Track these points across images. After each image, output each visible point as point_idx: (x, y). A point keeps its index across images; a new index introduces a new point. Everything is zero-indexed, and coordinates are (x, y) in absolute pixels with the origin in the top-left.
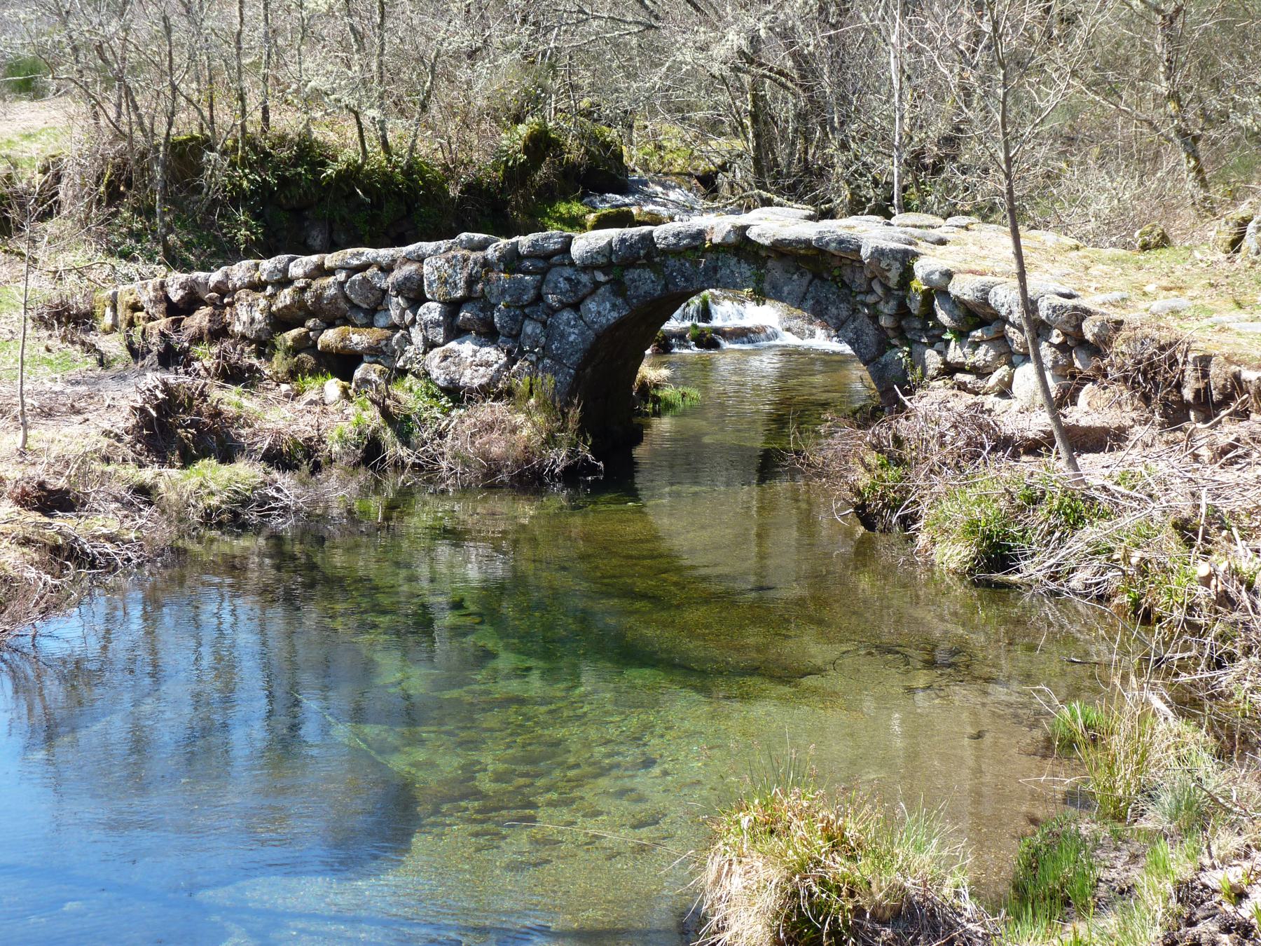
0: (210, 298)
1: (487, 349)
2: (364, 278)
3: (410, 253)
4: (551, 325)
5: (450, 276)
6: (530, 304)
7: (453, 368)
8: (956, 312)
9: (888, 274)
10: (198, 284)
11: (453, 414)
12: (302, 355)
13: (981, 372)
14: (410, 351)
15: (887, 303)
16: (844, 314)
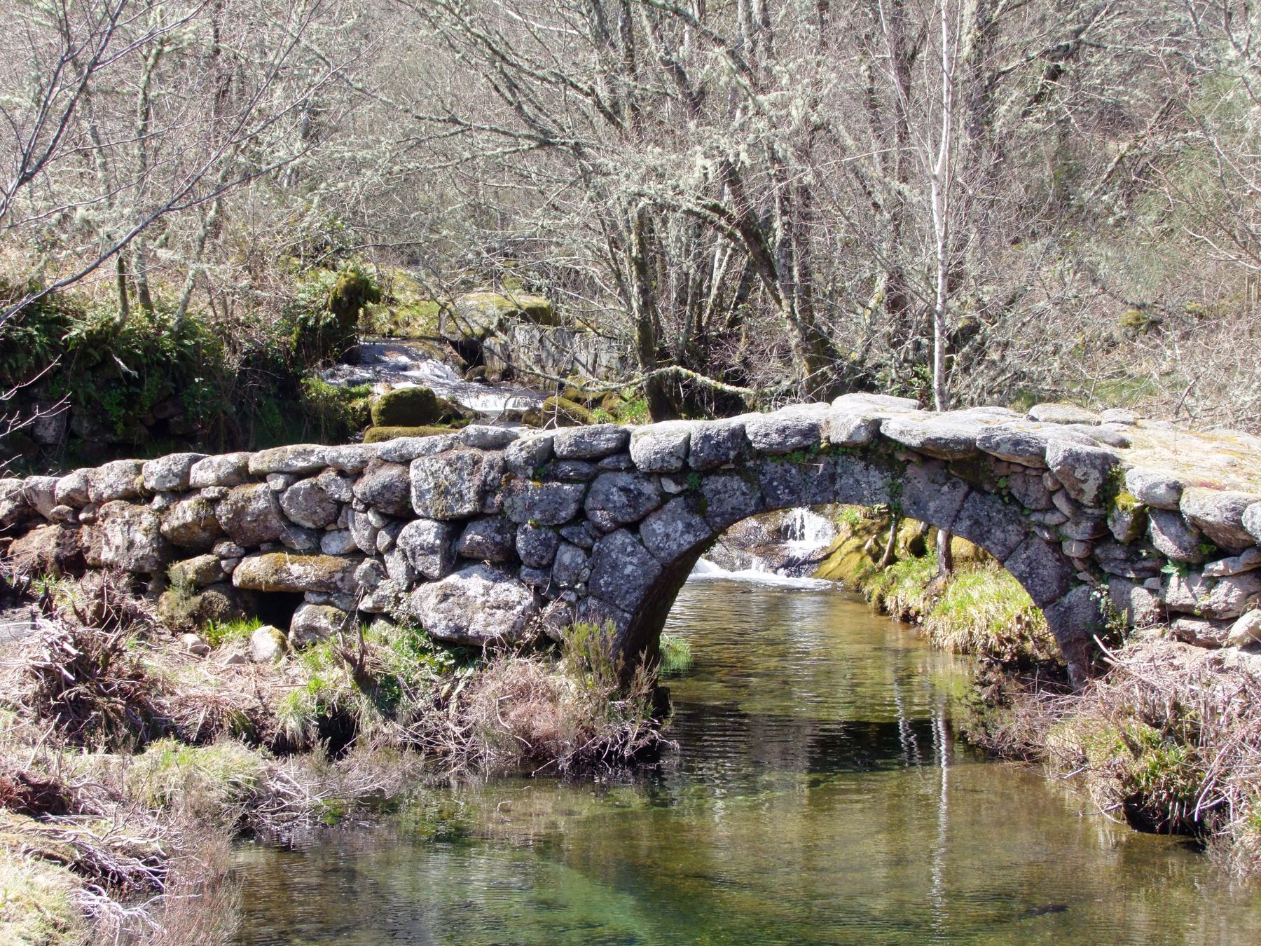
0: (58, 513)
1: (505, 585)
2: (313, 486)
3: (389, 452)
4: (599, 552)
5: (454, 484)
6: (568, 523)
7: (458, 612)
8: (1187, 538)
9: (1084, 487)
10: (37, 493)
11: (458, 674)
12: (210, 593)
13: (1220, 619)
14: (386, 588)
15: (1077, 524)
16: (1013, 539)
